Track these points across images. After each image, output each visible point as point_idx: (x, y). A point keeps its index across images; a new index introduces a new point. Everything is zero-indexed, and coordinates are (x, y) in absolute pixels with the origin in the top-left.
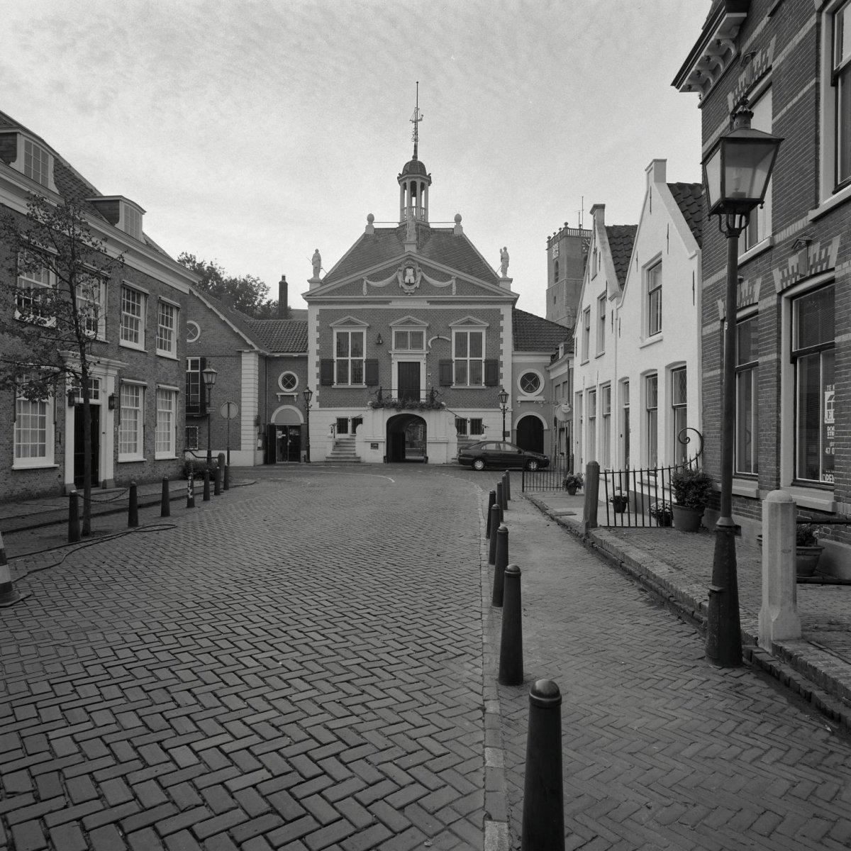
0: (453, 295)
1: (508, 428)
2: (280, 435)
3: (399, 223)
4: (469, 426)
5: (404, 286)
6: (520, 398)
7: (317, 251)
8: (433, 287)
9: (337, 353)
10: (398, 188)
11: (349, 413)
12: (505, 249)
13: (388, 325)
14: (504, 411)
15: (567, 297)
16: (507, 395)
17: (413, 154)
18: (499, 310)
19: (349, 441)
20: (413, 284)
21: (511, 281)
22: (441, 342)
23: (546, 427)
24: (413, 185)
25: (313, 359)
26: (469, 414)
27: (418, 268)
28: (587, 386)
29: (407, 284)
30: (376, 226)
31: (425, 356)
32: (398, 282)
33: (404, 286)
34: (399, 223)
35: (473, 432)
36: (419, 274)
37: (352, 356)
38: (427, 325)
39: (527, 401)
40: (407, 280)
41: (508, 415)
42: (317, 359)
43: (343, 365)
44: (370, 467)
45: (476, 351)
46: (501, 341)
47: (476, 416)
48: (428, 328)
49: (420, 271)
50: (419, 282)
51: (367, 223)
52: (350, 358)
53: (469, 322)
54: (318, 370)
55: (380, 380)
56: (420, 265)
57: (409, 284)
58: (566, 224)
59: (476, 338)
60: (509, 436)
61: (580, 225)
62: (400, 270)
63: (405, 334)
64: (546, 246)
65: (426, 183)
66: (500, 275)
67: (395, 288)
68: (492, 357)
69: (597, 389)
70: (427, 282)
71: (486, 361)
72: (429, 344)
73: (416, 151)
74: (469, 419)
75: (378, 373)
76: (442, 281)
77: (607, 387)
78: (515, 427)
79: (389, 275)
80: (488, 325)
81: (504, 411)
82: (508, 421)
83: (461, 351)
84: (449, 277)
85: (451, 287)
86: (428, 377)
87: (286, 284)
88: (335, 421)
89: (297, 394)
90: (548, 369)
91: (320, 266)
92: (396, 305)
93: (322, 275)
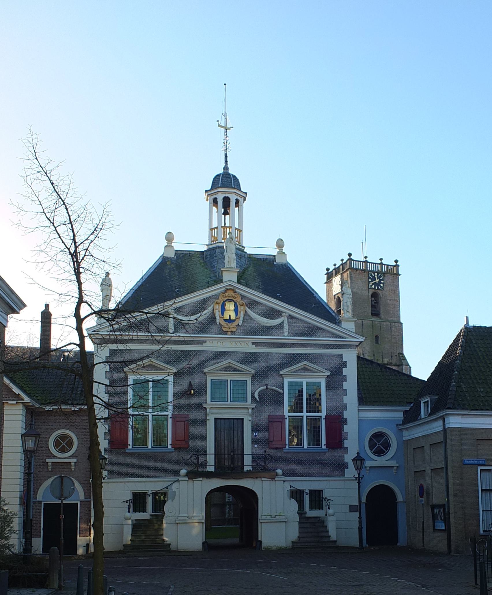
0: (285, 337)
3: (207, 245)
4: (307, 498)
5: (223, 323)
8: (258, 325)
9: (300, 412)
10: (206, 204)
18: (341, 356)
23: (400, 498)
24: (226, 202)
31: (250, 411)
33: (223, 323)
34: (207, 245)
36: (241, 309)
37: (302, 412)
39: (384, 467)
50: (241, 319)
51: (165, 243)
56: (243, 297)
57: (230, 321)
58: (350, 255)
62: (217, 303)
65: (241, 200)
68: (334, 413)
70: (251, 319)
71: (327, 418)
72: (256, 395)
73: (226, 162)
78: (364, 500)
80: (329, 374)
84: (279, 314)
85: (281, 325)
86: (254, 437)
87: (50, 315)
88: (129, 497)
89: (75, 460)
90: (401, 427)
93: (112, 306)
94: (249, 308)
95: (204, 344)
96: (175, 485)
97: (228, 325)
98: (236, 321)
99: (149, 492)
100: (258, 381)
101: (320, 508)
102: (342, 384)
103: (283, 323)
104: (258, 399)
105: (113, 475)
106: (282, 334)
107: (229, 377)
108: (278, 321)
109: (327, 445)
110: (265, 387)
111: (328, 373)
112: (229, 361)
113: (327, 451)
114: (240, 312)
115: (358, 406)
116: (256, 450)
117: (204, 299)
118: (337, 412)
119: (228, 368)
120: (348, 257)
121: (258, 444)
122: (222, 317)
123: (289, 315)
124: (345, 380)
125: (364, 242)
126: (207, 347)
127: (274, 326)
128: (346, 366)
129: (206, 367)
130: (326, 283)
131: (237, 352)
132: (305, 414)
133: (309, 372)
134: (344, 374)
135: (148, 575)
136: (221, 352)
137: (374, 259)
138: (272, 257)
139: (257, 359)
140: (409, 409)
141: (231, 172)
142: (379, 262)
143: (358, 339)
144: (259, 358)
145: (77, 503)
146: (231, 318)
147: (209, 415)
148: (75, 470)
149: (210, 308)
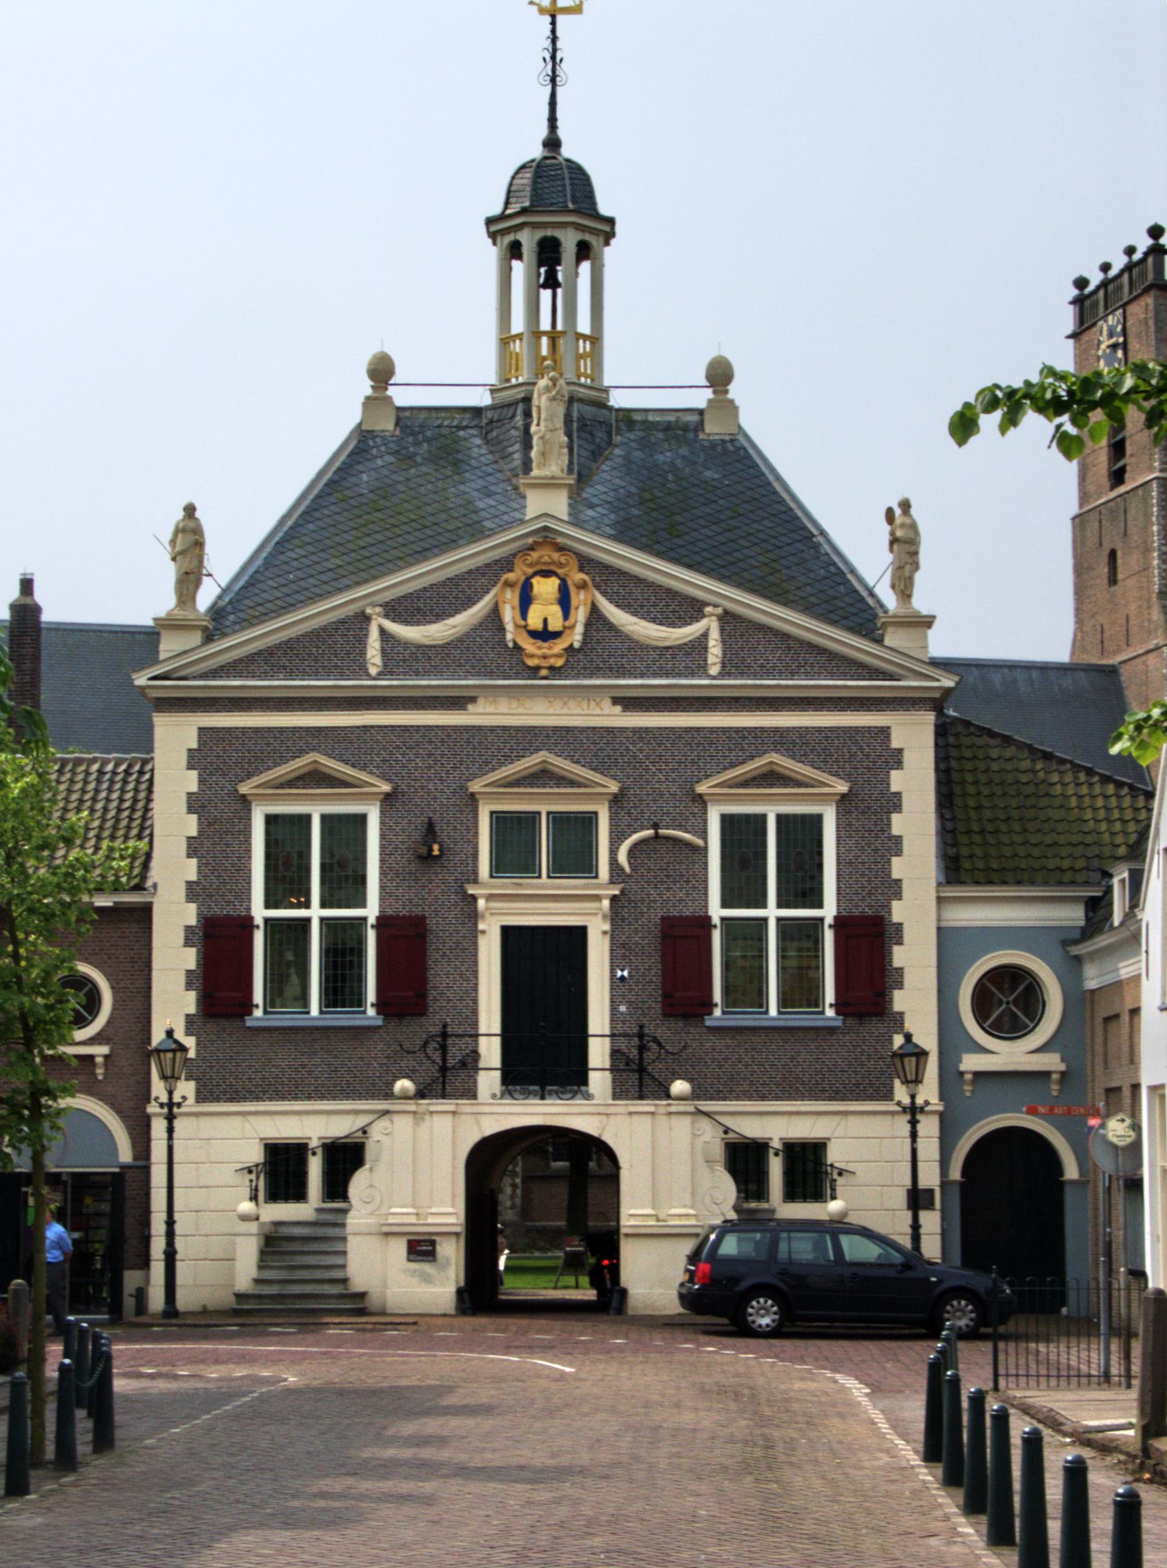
4: (776, 1168)
5: (528, 645)
10: (489, 254)
18: (884, 732)
20: (557, 635)
24: (549, 253)
31: (606, 903)
47: (803, 1129)
50: (580, 629)
51: (365, 387)
56: (586, 563)
57: (544, 635)
62: (508, 584)
68: (864, 908)
70: (611, 627)
71: (840, 924)
84: (691, 609)
85: (700, 644)
86: (617, 984)
88: (256, 1155)
89: (105, 1050)
94: (604, 594)
95: (470, 707)
96: (383, 1124)
97: (540, 648)
98: (564, 636)
99: (314, 1143)
100: (629, 814)
101: (817, 1195)
102: (889, 820)
103: (705, 635)
104: (628, 870)
105: (212, 1093)
106: (701, 669)
108: (691, 631)
109: (839, 1006)
110: (651, 832)
111: (842, 787)
112: (542, 755)
113: (839, 1023)
114: (577, 608)
115: (939, 884)
116: (624, 1022)
117: (470, 572)
118: (870, 906)
119: (542, 776)
120: (1150, 242)
121: (630, 1003)
122: (523, 623)
123: (726, 612)
124: (898, 807)
126: (479, 715)
127: (680, 647)
128: (899, 764)
129: (475, 776)
130: (1074, 336)
131: (568, 729)
132: (772, 912)
133: (786, 786)
134: (894, 788)
136: (518, 729)
139: (627, 749)
140: (1100, 894)
143: (938, 680)
144: (634, 743)
145: (579, 934)
146: (551, 628)
147: (483, 916)
148: (105, 1078)
149: (487, 600)
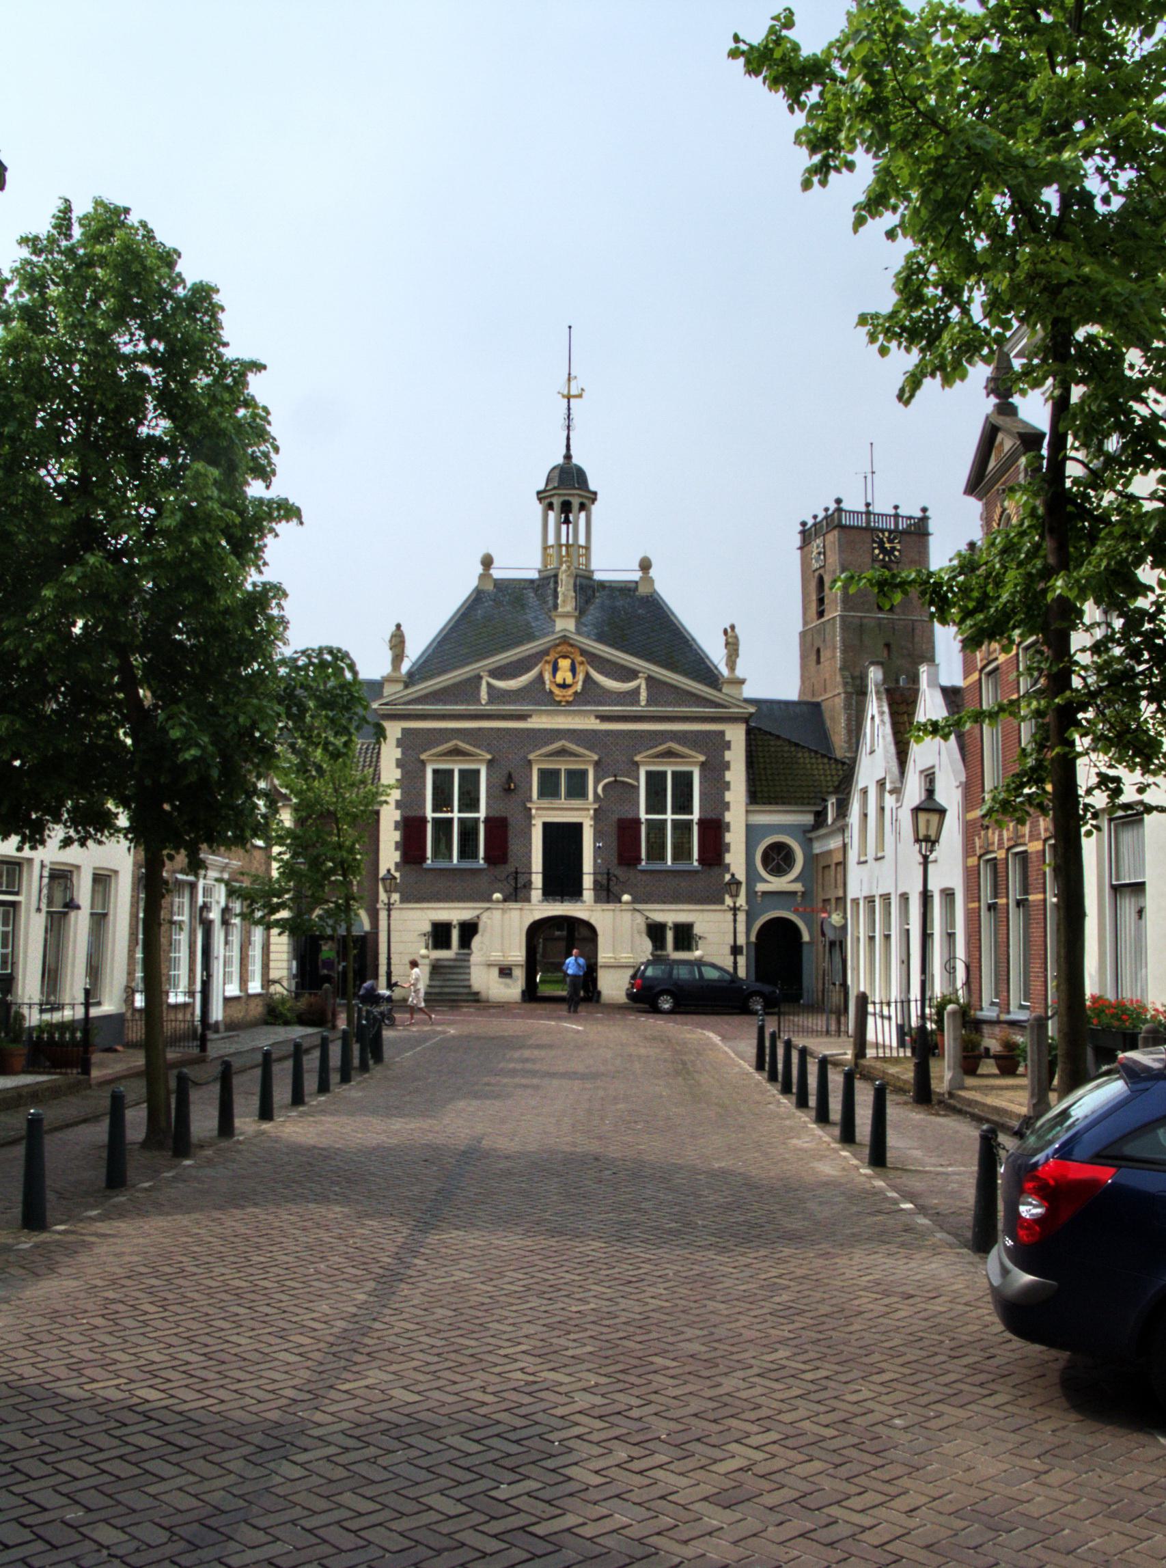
0: (642, 706)
1: (741, 940)
2: (327, 951)
4: (670, 936)
5: (556, 691)
6: (761, 887)
7: (398, 626)
10: (538, 508)
11: (455, 913)
12: (733, 627)
13: (525, 757)
14: (735, 910)
15: (844, 652)
16: (739, 883)
17: (564, 451)
18: (722, 733)
19: (458, 964)
20: (569, 686)
21: (742, 682)
22: (621, 791)
23: (806, 937)
25: (389, 816)
26: (670, 915)
27: (580, 659)
28: (865, 894)
29: (559, 686)
30: (496, 574)
31: (592, 812)
32: (544, 683)
35: (677, 947)
38: (596, 758)
40: (559, 679)
41: (741, 917)
42: (397, 815)
43: (443, 826)
44: (502, 1008)
45: (683, 805)
46: (727, 786)
48: (597, 764)
49: (582, 663)
50: (580, 683)
51: (480, 569)
52: (456, 815)
53: (670, 754)
54: (397, 836)
55: (510, 854)
56: (583, 652)
57: (564, 686)
58: (838, 501)
59: (683, 781)
60: (741, 953)
61: (868, 505)
62: (547, 662)
63: (556, 773)
64: (797, 540)
66: (725, 671)
67: (538, 694)
69: (877, 900)
71: (701, 822)
74: (670, 924)
75: (506, 842)
76: (623, 681)
77: (886, 898)
78: (753, 939)
79: (528, 670)
81: (735, 910)
82: (741, 927)
83: (656, 804)
84: (631, 674)
85: (636, 691)
86: (597, 851)
88: (428, 928)
91: (403, 651)
92: (539, 722)
93: (406, 666)
99: (455, 922)
106: (637, 703)
107: (563, 766)
119: (562, 752)
125: (869, 476)
129: (531, 752)
135: (877, 859)
137: (882, 506)
138: (633, 585)
141: (576, 460)
142: (892, 512)
